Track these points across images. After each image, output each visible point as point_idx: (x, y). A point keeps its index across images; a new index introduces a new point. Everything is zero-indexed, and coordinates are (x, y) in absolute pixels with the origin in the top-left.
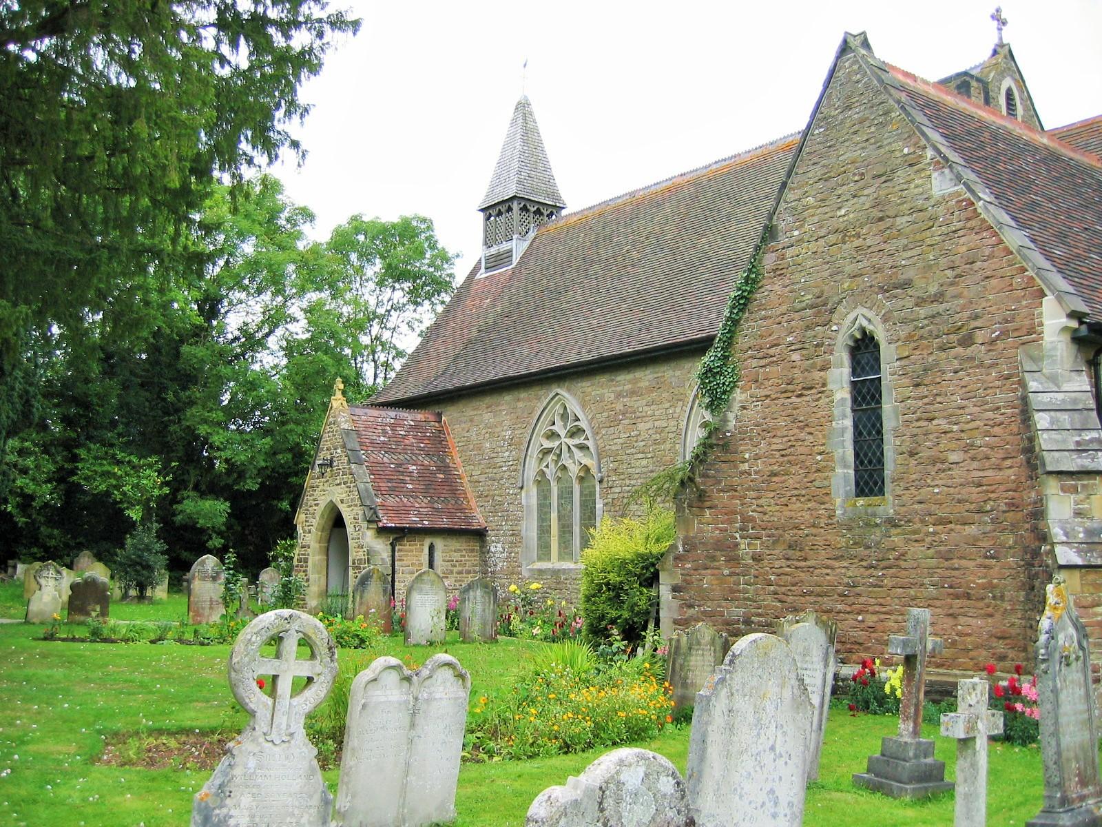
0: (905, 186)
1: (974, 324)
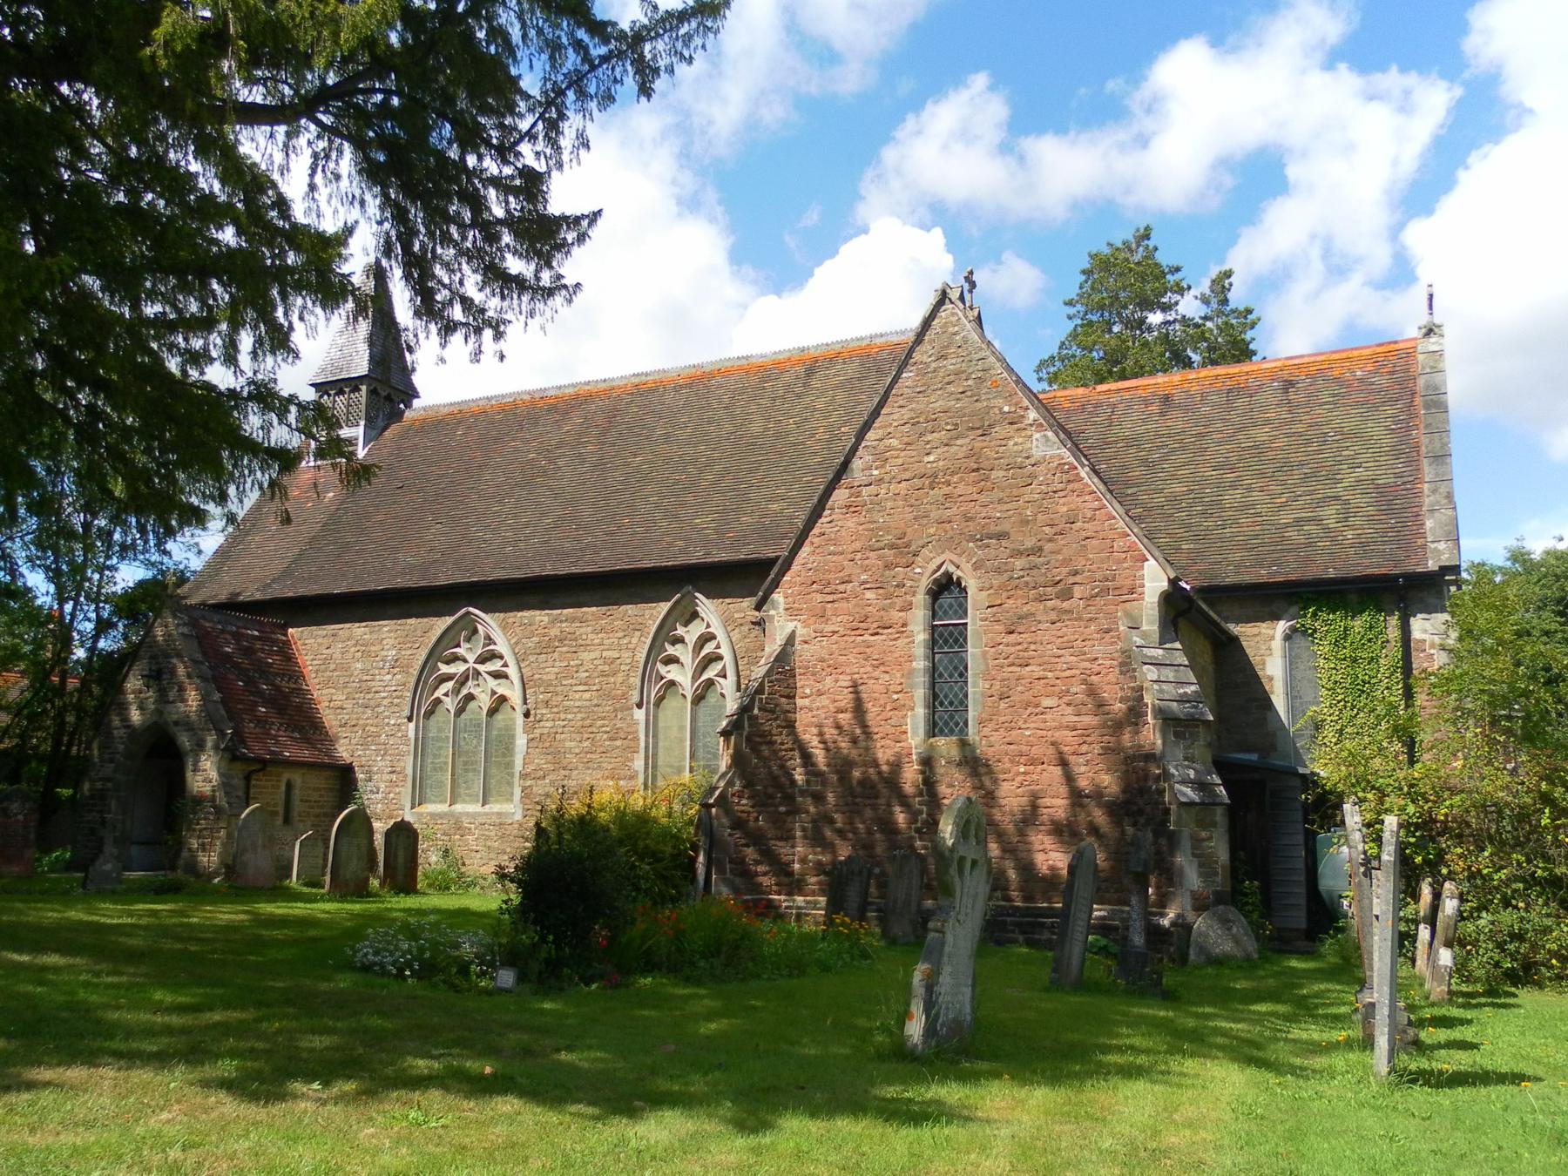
0: (1004, 442)
1: (1071, 580)
